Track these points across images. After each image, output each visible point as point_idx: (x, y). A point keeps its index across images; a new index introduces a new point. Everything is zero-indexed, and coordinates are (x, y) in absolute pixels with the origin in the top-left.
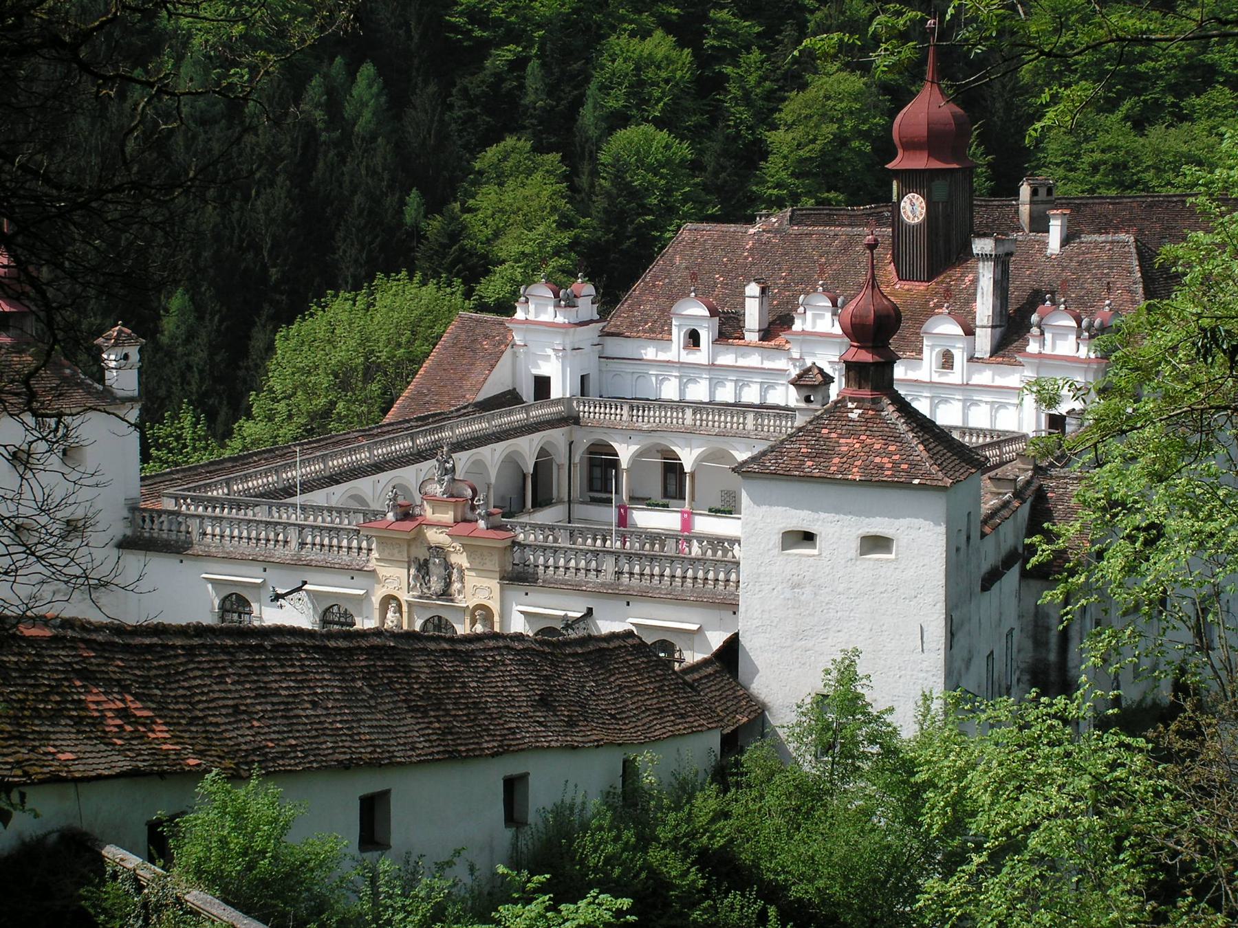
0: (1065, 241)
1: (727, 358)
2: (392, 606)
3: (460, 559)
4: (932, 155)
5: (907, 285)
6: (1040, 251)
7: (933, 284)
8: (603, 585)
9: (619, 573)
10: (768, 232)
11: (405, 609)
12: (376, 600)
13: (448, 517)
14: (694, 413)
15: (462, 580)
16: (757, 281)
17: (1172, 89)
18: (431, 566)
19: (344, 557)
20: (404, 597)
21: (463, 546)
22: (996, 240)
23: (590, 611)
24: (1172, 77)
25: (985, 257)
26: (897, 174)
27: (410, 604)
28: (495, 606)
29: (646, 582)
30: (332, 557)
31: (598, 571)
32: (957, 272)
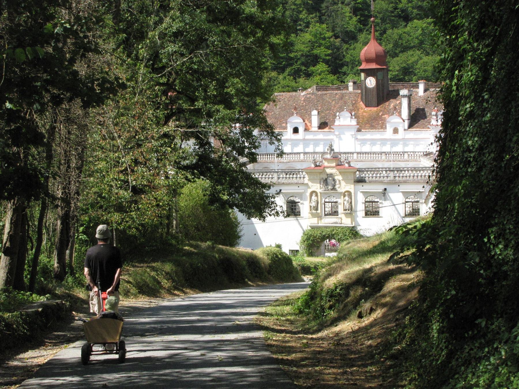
0: (426, 90)
1: (309, 136)
2: (314, 195)
3: (338, 177)
4: (377, 63)
5: (369, 109)
6: (416, 95)
7: (379, 108)
8: (390, 181)
9: (395, 177)
10: (309, 94)
11: (319, 194)
12: (308, 194)
13: (334, 164)
14: (304, 155)
15: (340, 183)
16: (316, 109)
17: (303, 64)
18: (328, 181)
19: (295, 180)
20: (319, 191)
21: (340, 172)
22: (409, 90)
23: (385, 189)
24: (303, 59)
25: (404, 96)
26: (363, 71)
27: (321, 193)
28: (352, 191)
29: (404, 179)
30: (291, 181)
31: (387, 177)
32: (387, 103)
